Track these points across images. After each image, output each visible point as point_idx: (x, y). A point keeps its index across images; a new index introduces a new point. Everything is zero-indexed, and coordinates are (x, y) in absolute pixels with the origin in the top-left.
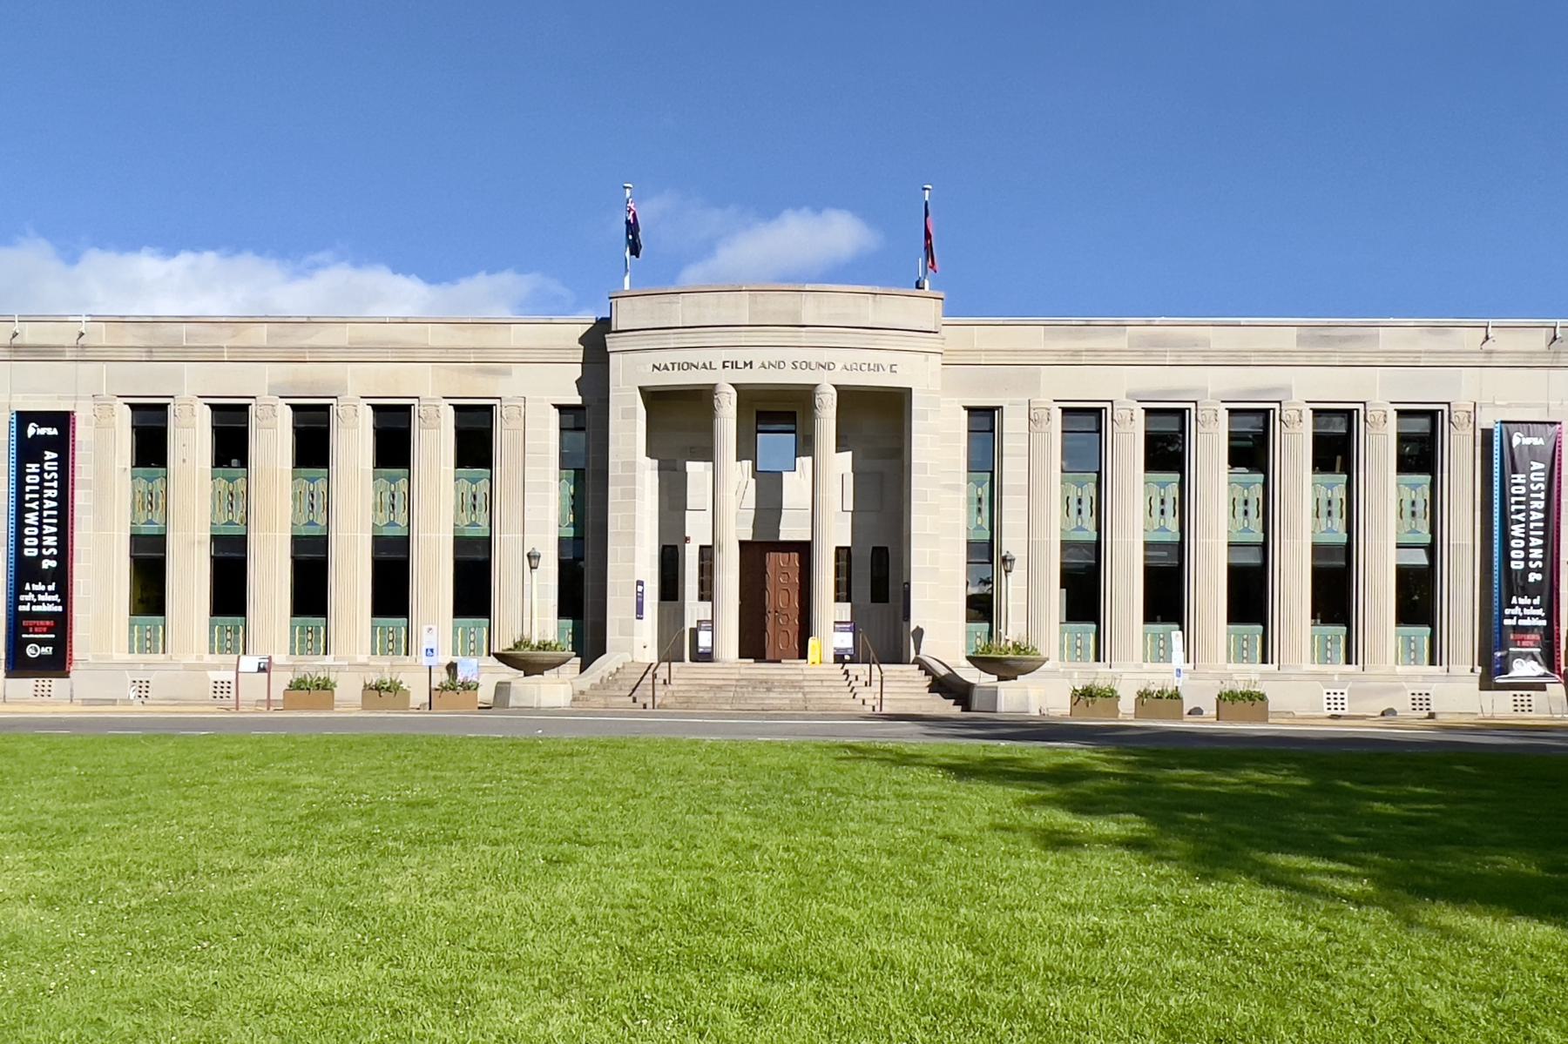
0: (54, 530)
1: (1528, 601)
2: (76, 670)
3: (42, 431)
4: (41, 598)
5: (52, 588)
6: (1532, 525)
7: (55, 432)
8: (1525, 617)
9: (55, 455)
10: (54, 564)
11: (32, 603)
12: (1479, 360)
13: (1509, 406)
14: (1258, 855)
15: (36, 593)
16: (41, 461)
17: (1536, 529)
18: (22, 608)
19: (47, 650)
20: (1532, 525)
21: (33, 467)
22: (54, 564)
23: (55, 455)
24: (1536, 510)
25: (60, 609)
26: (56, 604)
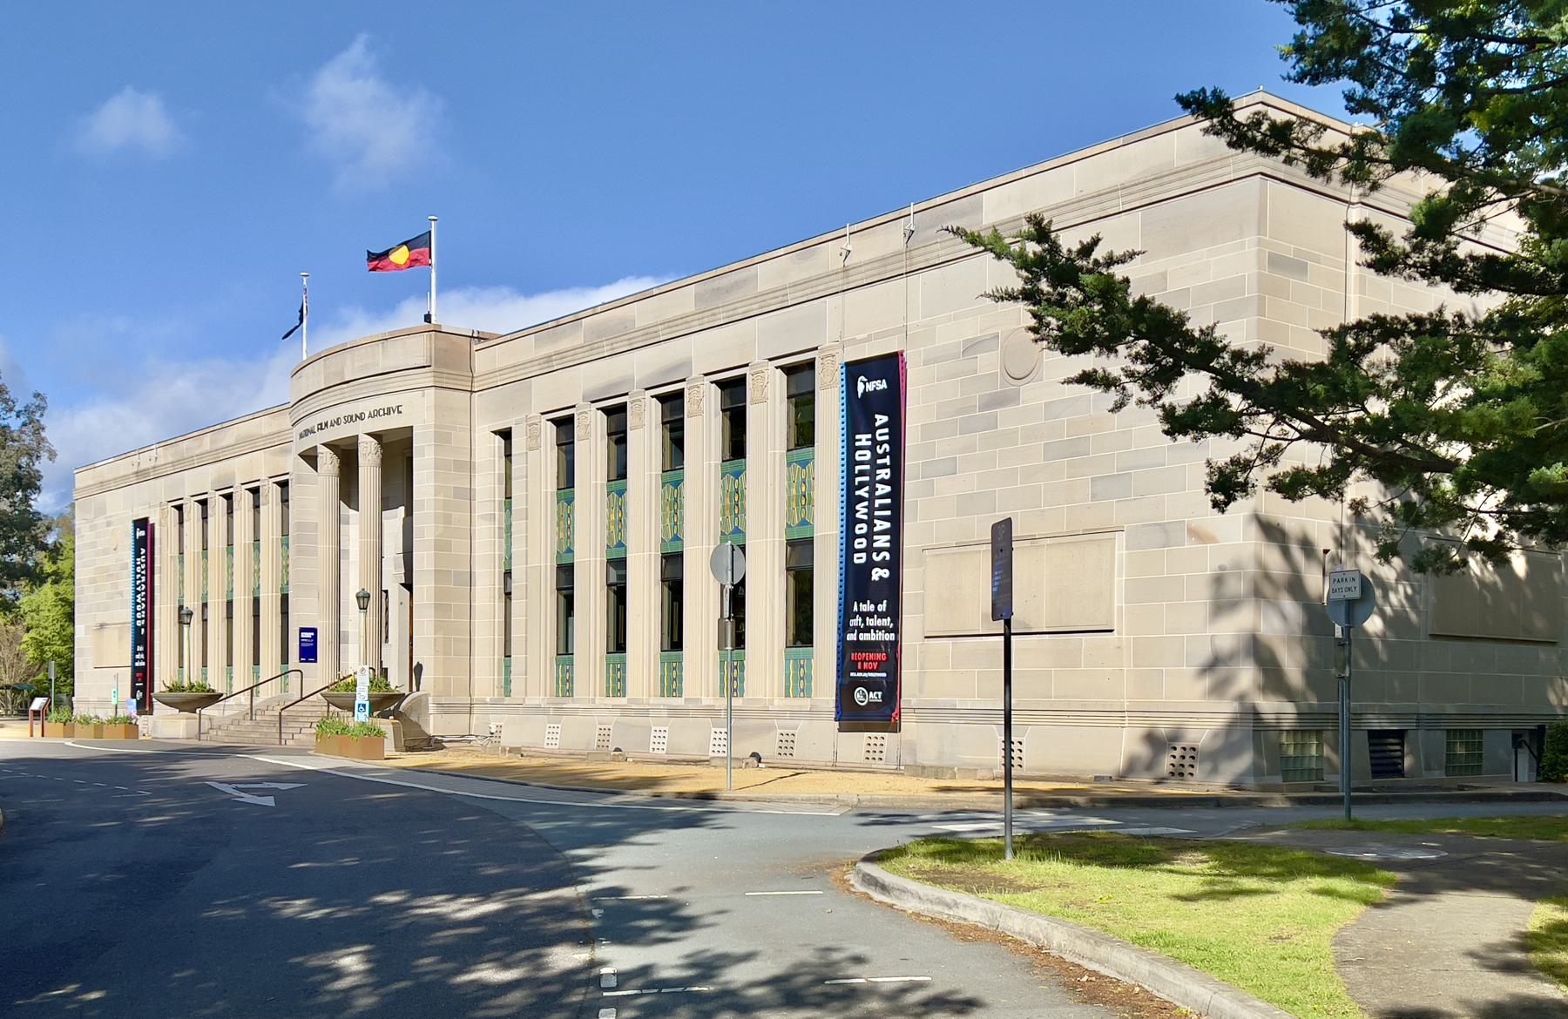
0: (887, 525)
1: (872, 608)
2: (908, 723)
3: (870, 387)
4: (870, 622)
5: (882, 607)
6: (878, 502)
7: (882, 385)
8: (867, 630)
9: (885, 419)
10: (885, 573)
11: (860, 630)
12: (838, 283)
13: (868, 339)
14: (423, 944)
15: (864, 615)
16: (872, 430)
17: (883, 507)
18: (851, 637)
19: (875, 696)
20: (878, 502)
21: (863, 439)
22: (885, 573)
23: (885, 419)
24: (883, 482)
25: (891, 637)
26: (887, 630)
